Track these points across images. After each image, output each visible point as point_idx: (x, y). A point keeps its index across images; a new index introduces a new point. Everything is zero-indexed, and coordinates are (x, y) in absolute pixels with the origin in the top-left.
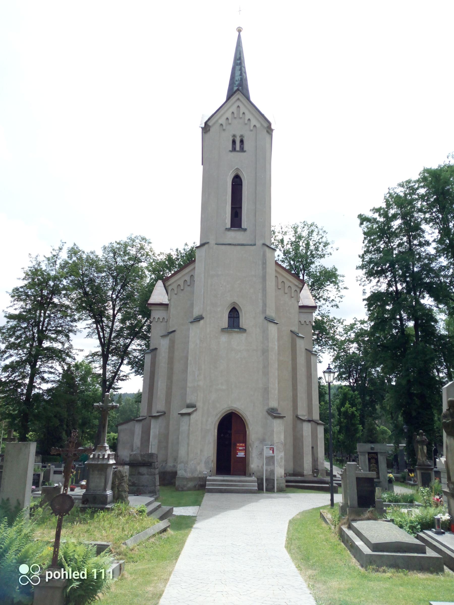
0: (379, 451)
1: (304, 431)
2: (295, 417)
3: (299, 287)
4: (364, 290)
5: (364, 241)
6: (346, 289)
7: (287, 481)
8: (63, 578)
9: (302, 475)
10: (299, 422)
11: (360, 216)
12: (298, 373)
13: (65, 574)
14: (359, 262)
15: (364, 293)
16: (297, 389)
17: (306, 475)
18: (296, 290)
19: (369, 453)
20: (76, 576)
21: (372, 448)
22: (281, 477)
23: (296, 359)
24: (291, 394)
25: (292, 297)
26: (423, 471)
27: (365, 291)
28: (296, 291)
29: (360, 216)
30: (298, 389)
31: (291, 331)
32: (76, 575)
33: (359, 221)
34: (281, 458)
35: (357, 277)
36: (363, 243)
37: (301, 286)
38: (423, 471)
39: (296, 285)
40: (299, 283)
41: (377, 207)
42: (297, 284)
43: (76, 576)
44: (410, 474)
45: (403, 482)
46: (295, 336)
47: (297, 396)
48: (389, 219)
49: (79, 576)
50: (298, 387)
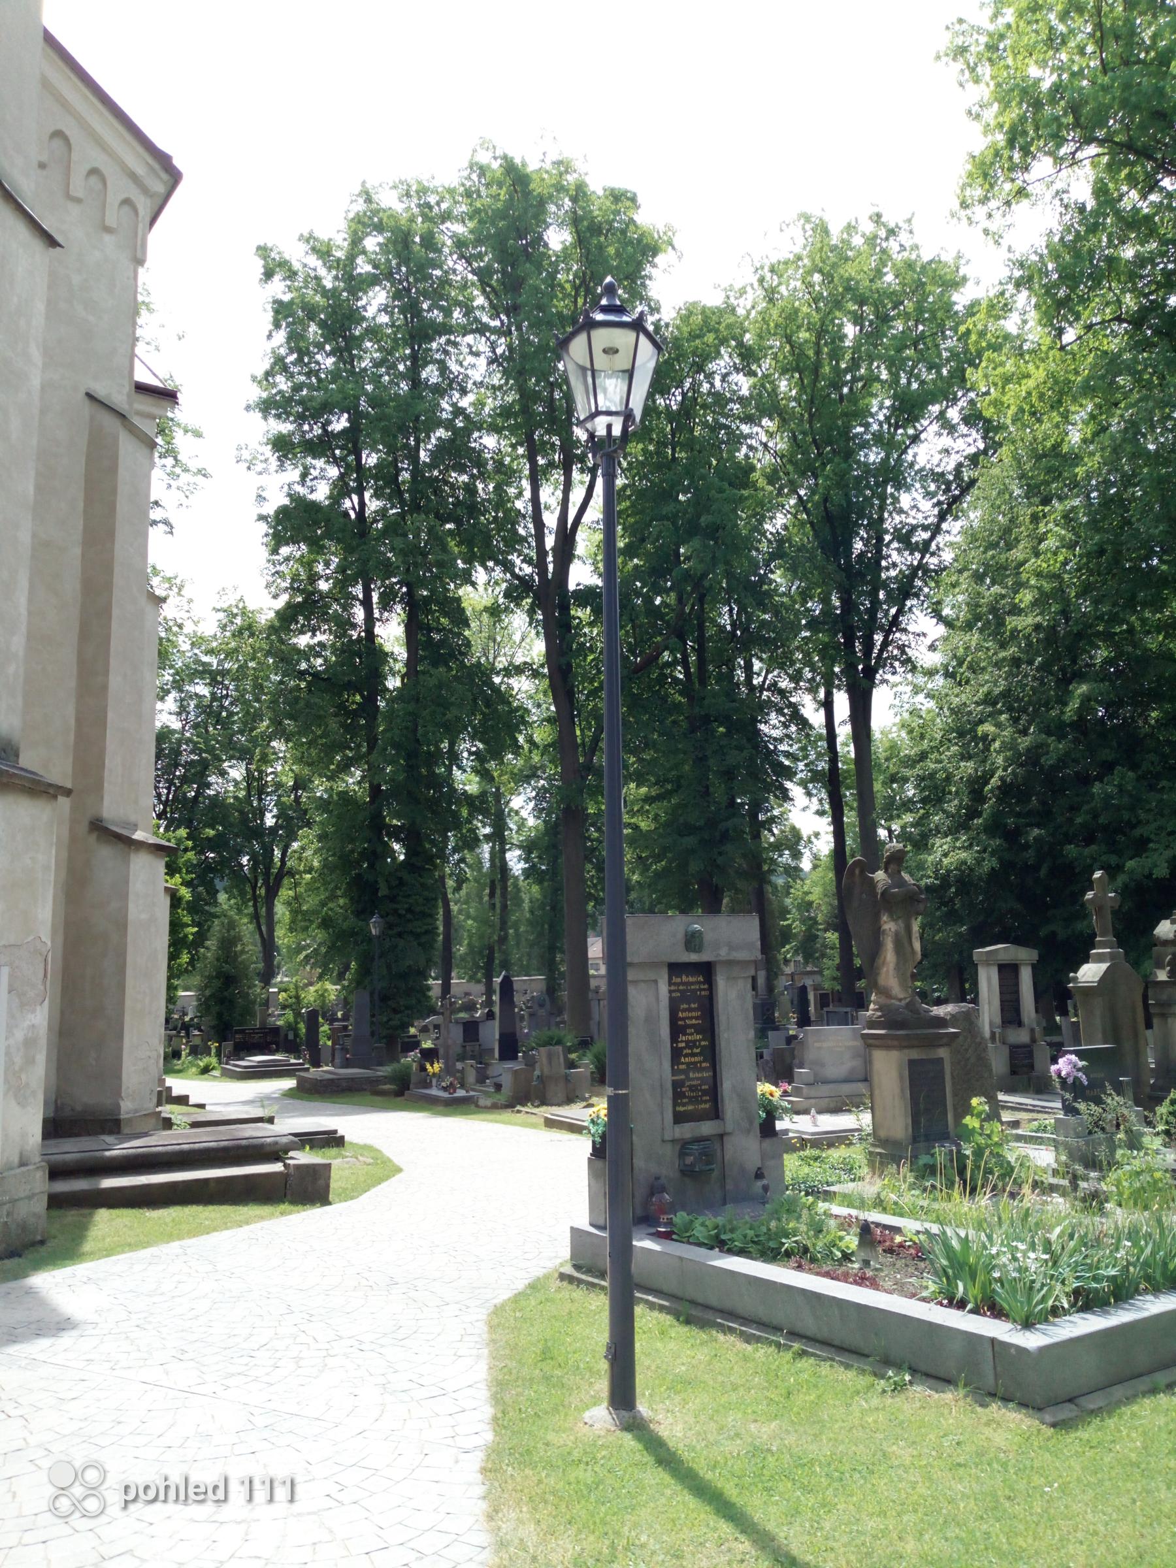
0: (723, 953)
1: (131, 897)
2: (84, 827)
3: (145, 190)
4: (262, 488)
5: (270, 332)
6: (204, 475)
7: (56, 1172)
8: (162, 1497)
9: (112, 1125)
10: (105, 853)
11: (263, 251)
12: (116, 612)
13: (167, 1487)
14: (257, 393)
15: (261, 498)
16: (105, 688)
17: (129, 1120)
18: (127, 202)
19: (675, 968)
20: (196, 1494)
21: (692, 941)
22: (23, 1164)
23: (111, 535)
24: (70, 710)
25: (108, 230)
26: (915, 1054)
27: (264, 494)
28: (126, 208)
29: (263, 251)
30: (110, 689)
31: (90, 396)
32: (197, 1490)
33: (258, 266)
34: (29, 1043)
35: (239, 448)
36: (270, 336)
37: (160, 188)
38: (915, 1054)
39: (133, 177)
40: (152, 169)
41: (323, 235)
42: (140, 170)
43: (196, 1494)
44: (428, 1066)
45: (399, 1093)
46: (109, 422)
47: (102, 722)
48: (357, 285)
49: (206, 1493)
50: (111, 677)
